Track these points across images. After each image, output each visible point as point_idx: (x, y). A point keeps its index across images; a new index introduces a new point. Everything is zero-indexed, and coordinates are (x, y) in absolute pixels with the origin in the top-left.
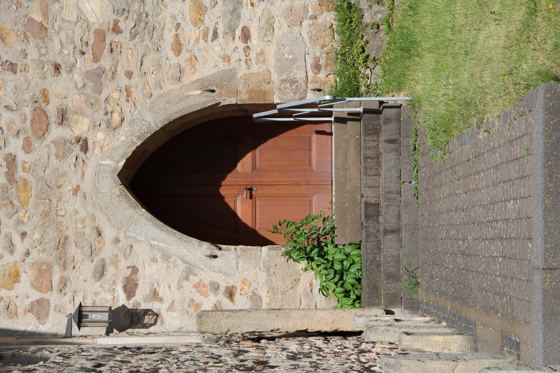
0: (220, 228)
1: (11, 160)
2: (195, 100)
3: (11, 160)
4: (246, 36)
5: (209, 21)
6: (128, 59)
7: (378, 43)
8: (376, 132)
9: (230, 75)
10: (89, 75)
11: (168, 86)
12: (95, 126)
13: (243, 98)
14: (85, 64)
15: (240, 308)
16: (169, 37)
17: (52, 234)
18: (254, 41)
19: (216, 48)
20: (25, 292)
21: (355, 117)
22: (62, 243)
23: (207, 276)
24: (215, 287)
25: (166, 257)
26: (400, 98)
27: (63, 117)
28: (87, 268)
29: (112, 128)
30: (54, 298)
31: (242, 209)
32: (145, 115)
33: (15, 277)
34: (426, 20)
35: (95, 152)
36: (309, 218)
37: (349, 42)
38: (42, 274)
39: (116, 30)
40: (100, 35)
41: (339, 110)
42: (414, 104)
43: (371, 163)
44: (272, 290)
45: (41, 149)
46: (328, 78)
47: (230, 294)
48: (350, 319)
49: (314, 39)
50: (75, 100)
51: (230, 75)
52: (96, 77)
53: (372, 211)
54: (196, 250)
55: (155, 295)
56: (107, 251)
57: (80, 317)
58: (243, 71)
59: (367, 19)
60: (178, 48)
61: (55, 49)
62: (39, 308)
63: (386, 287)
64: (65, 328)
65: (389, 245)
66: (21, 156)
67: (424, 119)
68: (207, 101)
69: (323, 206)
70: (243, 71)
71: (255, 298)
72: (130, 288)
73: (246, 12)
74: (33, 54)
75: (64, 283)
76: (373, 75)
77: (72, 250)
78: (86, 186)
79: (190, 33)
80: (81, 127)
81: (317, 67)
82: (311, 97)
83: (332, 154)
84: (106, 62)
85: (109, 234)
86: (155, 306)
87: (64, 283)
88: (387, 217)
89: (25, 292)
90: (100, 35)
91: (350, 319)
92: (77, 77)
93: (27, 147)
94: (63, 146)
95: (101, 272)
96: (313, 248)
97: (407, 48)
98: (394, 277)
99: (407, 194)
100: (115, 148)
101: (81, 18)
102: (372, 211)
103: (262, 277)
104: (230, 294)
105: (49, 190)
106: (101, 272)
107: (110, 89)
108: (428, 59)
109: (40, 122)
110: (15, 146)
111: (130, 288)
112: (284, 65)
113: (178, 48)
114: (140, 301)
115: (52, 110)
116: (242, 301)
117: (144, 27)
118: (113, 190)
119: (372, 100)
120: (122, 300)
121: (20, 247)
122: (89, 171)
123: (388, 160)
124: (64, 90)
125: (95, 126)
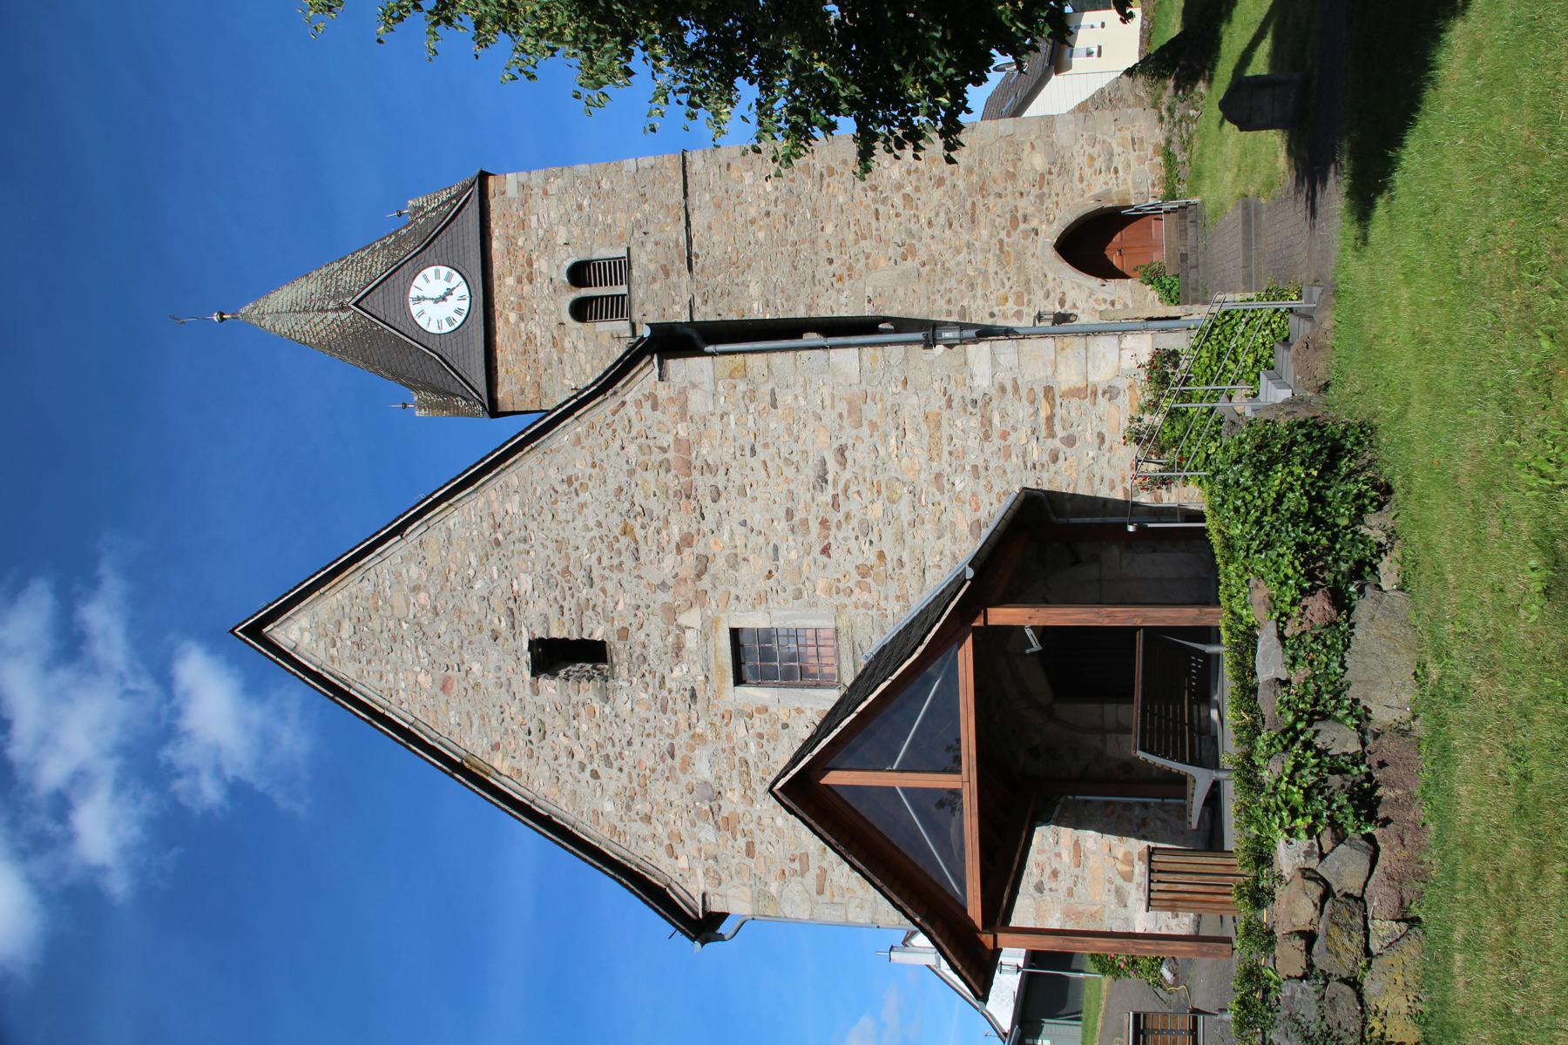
0: (1106, 271)
1: (1001, 242)
2: (1092, 206)
3: (1001, 242)
4: (1116, 171)
5: (1097, 165)
6: (1057, 187)
7: (1185, 172)
8: (1185, 217)
9: (1109, 192)
10: (1037, 196)
11: (1078, 200)
12: (1041, 222)
13: (1115, 203)
14: (1035, 191)
15: (471, 743)
16: (1077, 175)
17: (1022, 278)
18: (1121, 173)
19: (1101, 178)
20: (1011, 306)
21: (1174, 210)
22: (1028, 282)
23: (1100, 296)
24: (1105, 301)
25: (1080, 286)
26: (1197, 200)
27: (1025, 219)
28: (1041, 294)
29: (1050, 223)
30: (1025, 309)
31: (1116, 261)
32: (1065, 216)
33: (1006, 300)
34: (1207, 162)
35: (1041, 235)
36: (1152, 263)
37: (1170, 171)
38: (1019, 297)
39: (1050, 173)
40: (1042, 176)
41: (1166, 207)
42: (1203, 203)
43: (1183, 233)
44: (1134, 301)
45: (1015, 235)
46: (1160, 191)
47: (1113, 304)
48: (1174, 311)
49: (1151, 171)
50: (1030, 210)
51: (1109, 192)
52: (1041, 197)
53: (1184, 257)
54: (1093, 282)
55: (1074, 306)
56: (1050, 285)
57: (1039, 317)
58: (1115, 189)
59: (1179, 159)
60: (1081, 180)
61: (1021, 184)
62: (1018, 315)
63: (1192, 294)
64: (887, 835)
65: (1193, 274)
66: (1006, 240)
67: (1208, 210)
68: (1097, 206)
69: (1159, 257)
70: (1115, 189)
71: (1126, 306)
72: (1062, 303)
73: (1116, 159)
74: (1010, 188)
75: (1029, 301)
76: (1182, 189)
77: (1033, 285)
78: (1038, 252)
79: (1088, 172)
80: (1034, 223)
81: (1153, 185)
82: (1151, 201)
83: (1162, 230)
84: (1046, 189)
85: (1050, 276)
86: (1075, 311)
87: (1029, 301)
88: (1191, 260)
89: (1011, 306)
90: (1042, 176)
91: (1174, 311)
92: (1032, 198)
93: (1009, 235)
94: (1026, 234)
95: (1047, 295)
96: (1153, 277)
97: (1199, 175)
98: (1196, 290)
99: (1201, 248)
100: (1051, 234)
101: (1033, 168)
102: (1184, 257)
103: (1129, 294)
104: (1113, 304)
105: (1020, 256)
106: (1047, 295)
107: (1048, 203)
108: (1208, 181)
109: (1014, 222)
110: (1003, 235)
111: (1062, 303)
112: (1136, 185)
113: (1081, 180)
114: (1067, 309)
115: (1020, 215)
116: (1118, 306)
117: (1064, 170)
118: (1051, 253)
119: (1182, 201)
120: (1058, 309)
121: (1008, 284)
122: (1040, 244)
123: (1191, 231)
124: (1025, 205)
125: (1041, 222)
